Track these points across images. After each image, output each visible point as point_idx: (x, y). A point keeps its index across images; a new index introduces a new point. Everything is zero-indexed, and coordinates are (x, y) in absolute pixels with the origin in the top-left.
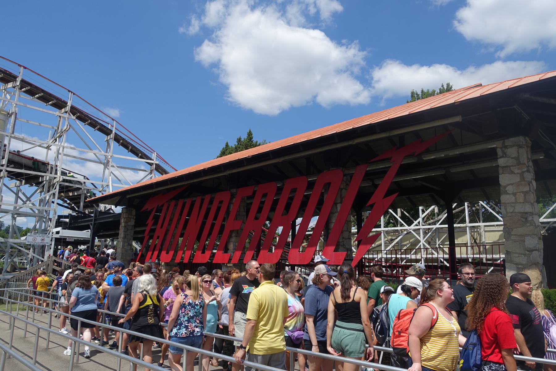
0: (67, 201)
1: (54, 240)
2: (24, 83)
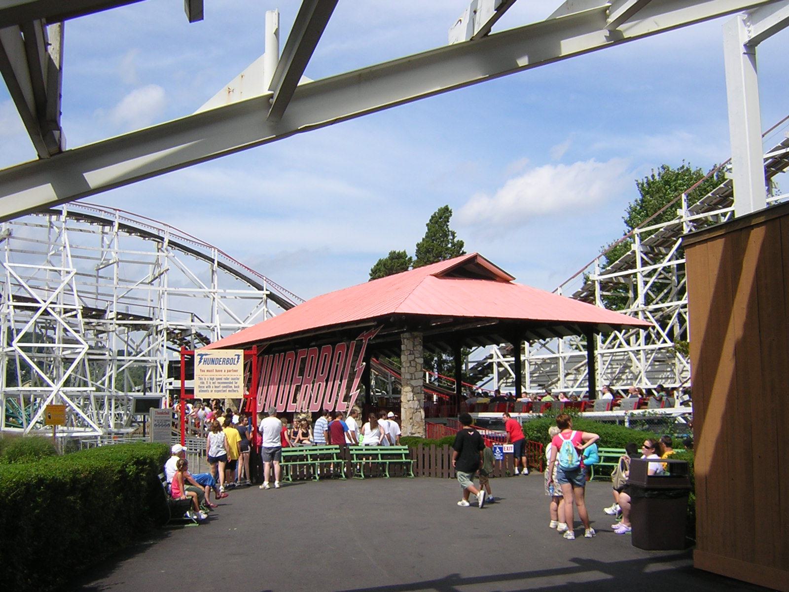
1: (168, 391)
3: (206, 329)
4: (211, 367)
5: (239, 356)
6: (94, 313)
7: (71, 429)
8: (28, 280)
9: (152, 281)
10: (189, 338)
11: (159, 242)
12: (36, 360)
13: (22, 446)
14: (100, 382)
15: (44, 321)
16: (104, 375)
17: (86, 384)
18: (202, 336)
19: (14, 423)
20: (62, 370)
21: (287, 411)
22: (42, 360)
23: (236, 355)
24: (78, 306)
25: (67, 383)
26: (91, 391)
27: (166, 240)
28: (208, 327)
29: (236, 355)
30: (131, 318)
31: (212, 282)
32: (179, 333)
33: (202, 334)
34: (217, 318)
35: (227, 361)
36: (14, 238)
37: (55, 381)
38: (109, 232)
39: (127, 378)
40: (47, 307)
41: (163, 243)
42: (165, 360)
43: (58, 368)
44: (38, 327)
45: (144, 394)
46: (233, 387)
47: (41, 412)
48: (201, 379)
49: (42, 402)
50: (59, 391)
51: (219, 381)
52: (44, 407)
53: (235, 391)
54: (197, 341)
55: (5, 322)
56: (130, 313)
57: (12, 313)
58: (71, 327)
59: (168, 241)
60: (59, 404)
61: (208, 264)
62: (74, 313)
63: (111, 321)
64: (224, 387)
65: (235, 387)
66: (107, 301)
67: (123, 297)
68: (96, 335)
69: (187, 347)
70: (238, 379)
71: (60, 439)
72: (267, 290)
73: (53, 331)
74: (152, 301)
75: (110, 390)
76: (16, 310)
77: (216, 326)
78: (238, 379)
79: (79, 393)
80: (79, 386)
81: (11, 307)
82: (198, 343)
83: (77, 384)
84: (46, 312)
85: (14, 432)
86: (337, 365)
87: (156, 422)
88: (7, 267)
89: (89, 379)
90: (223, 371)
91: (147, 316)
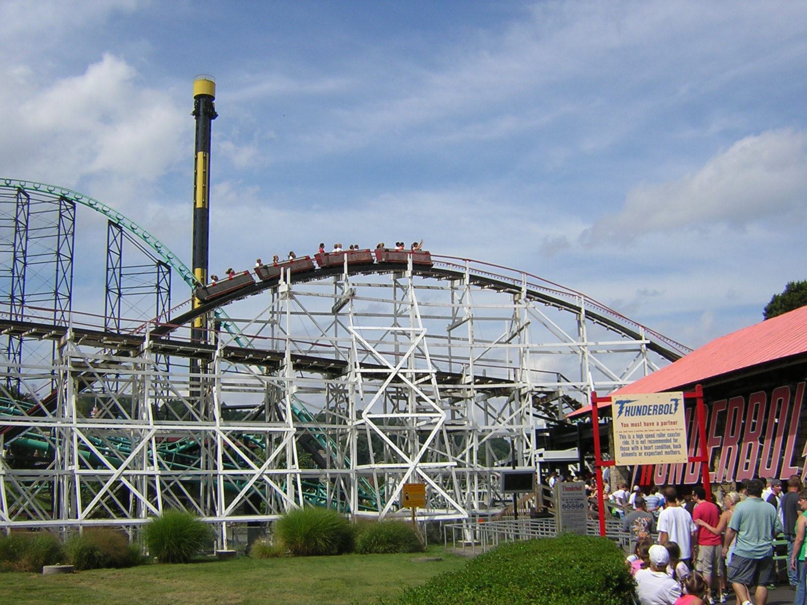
0: (541, 408)
1: (538, 465)
2: (473, 278)
3: (573, 390)
4: (637, 419)
5: (676, 400)
6: (449, 378)
7: (432, 511)
8: (376, 344)
9: (510, 340)
10: (554, 403)
11: (515, 293)
12: (388, 434)
13: (379, 533)
14: (460, 456)
15: (395, 390)
16: (464, 448)
17: (444, 459)
18: (571, 399)
19: (367, 504)
20: (417, 443)
21: (685, 483)
22: (395, 433)
23: (672, 400)
24: (432, 370)
25: (423, 460)
26: (451, 466)
27: (524, 290)
28: (575, 387)
29: (672, 400)
30: (490, 381)
31: (579, 335)
32: (544, 397)
33: (570, 397)
34: (589, 375)
35: (661, 409)
36: (357, 298)
37: (411, 456)
38: (460, 287)
39: (489, 451)
40: (398, 372)
41: (520, 294)
42: (532, 428)
43: (413, 442)
44: (389, 397)
45: (514, 468)
46: (672, 447)
47: (396, 493)
48: (623, 437)
49: (397, 482)
50: (416, 467)
51: (649, 439)
52: (399, 487)
53: (675, 453)
54: (565, 405)
55: (353, 392)
56: (487, 376)
57: (360, 382)
58: (427, 395)
59: (526, 291)
60: (416, 482)
61: (571, 316)
62: (427, 378)
63: (469, 386)
64: (658, 447)
65: (675, 447)
66: (463, 364)
67: (478, 359)
68: (452, 404)
69: (553, 413)
70: (678, 435)
71: (419, 523)
72: (646, 339)
73: (405, 401)
74: (511, 362)
75: (472, 465)
76: (364, 379)
77: (588, 386)
78: (678, 435)
79: (437, 470)
80: (437, 461)
81: (359, 375)
82: (566, 407)
83: (434, 459)
84: (397, 379)
85: (368, 516)
86: (744, 424)
87: (564, 503)
88: (352, 330)
89: (449, 454)
90: (655, 424)
91: (507, 379)
